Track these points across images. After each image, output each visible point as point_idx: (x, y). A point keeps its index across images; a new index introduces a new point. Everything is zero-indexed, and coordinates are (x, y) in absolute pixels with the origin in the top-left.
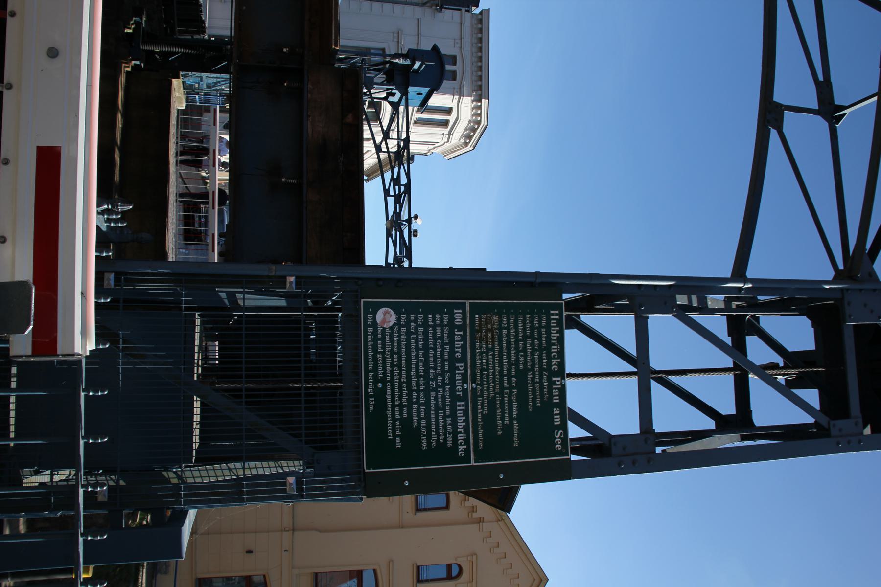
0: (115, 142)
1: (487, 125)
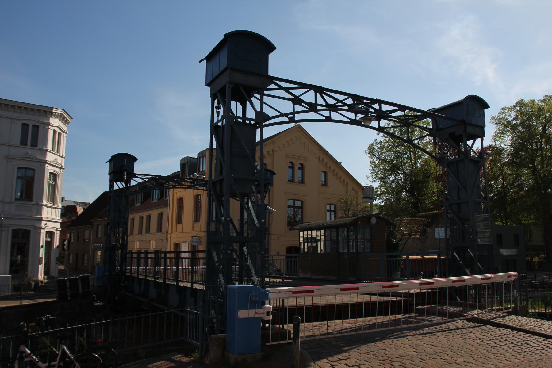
1: (64, 110)
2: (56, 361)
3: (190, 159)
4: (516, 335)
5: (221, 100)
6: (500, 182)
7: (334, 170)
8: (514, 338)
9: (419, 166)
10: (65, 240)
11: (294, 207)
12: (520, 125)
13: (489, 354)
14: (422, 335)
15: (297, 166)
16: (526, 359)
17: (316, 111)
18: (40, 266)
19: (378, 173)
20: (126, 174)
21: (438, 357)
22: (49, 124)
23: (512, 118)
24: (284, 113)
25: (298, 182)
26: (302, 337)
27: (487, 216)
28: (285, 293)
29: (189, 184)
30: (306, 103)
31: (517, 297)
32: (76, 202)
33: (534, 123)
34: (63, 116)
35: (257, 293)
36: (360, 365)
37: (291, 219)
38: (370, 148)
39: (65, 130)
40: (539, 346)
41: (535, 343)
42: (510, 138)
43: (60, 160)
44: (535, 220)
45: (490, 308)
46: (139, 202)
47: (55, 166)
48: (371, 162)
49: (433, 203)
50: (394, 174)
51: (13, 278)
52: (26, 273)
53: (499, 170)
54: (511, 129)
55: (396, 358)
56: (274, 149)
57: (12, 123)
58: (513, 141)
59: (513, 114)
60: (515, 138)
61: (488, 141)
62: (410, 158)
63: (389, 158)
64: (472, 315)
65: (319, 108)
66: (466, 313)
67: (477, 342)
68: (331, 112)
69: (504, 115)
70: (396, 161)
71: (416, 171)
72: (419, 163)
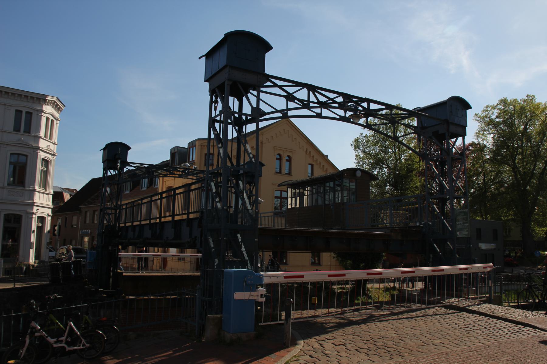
1: (57, 98)
2: (64, 336)
3: (180, 148)
4: (489, 321)
5: (219, 95)
6: (481, 178)
7: (320, 163)
8: (487, 324)
9: (403, 161)
10: (55, 226)
11: (281, 198)
12: (502, 123)
13: (464, 337)
14: (402, 320)
15: (285, 158)
16: (496, 341)
17: (309, 108)
18: (31, 250)
19: (363, 166)
20: (119, 162)
21: (417, 338)
22: (42, 111)
23: (495, 116)
24: (278, 109)
25: (286, 173)
26: (292, 319)
27: (466, 211)
28: (277, 278)
29: (181, 173)
30: (299, 100)
31: (492, 286)
32: (63, 189)
33: (515, 122)
34: (56, 104)
35: (252, 277)
36: (345, 344)
37: (277, 209)
38: (355, 142)
39: (58, 117)
40: (509, 331)
41: (505, 328)
42: (492, 136)
43: (52, 147)
44: (514, 216)
45: (466, 297)
46: (128, 189)
47: (48, 152)
48: (356, 156)
49: (416, 197)
50: (378, 167)
51: (5, 262)
52: (18, 257)
53: (481, 166)
54: (493, 127)
55: (379, 338)
56: (262, 141)
57: (5, 109)
58: (495, 139)
59: (496, 113)
60: (497, 136)
61: (470, 138)
62: (395, 152)
63: (373, 152)
64: (449, 303)
65: (311, 105)
66: (444, 301)
67: (453, 326)
68: (322, 109)
69: (487, 113)
70: (381, 155)
71: (400, 165)
72: (403, 157)
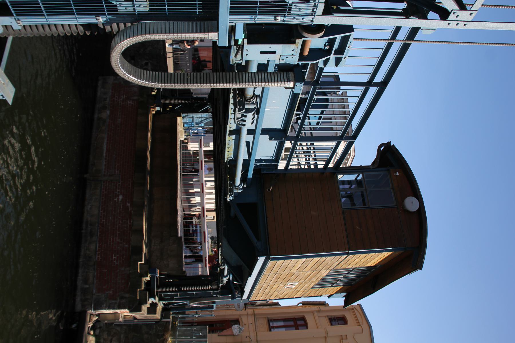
0: (147, 147)
